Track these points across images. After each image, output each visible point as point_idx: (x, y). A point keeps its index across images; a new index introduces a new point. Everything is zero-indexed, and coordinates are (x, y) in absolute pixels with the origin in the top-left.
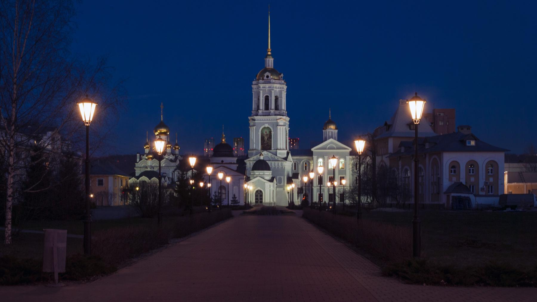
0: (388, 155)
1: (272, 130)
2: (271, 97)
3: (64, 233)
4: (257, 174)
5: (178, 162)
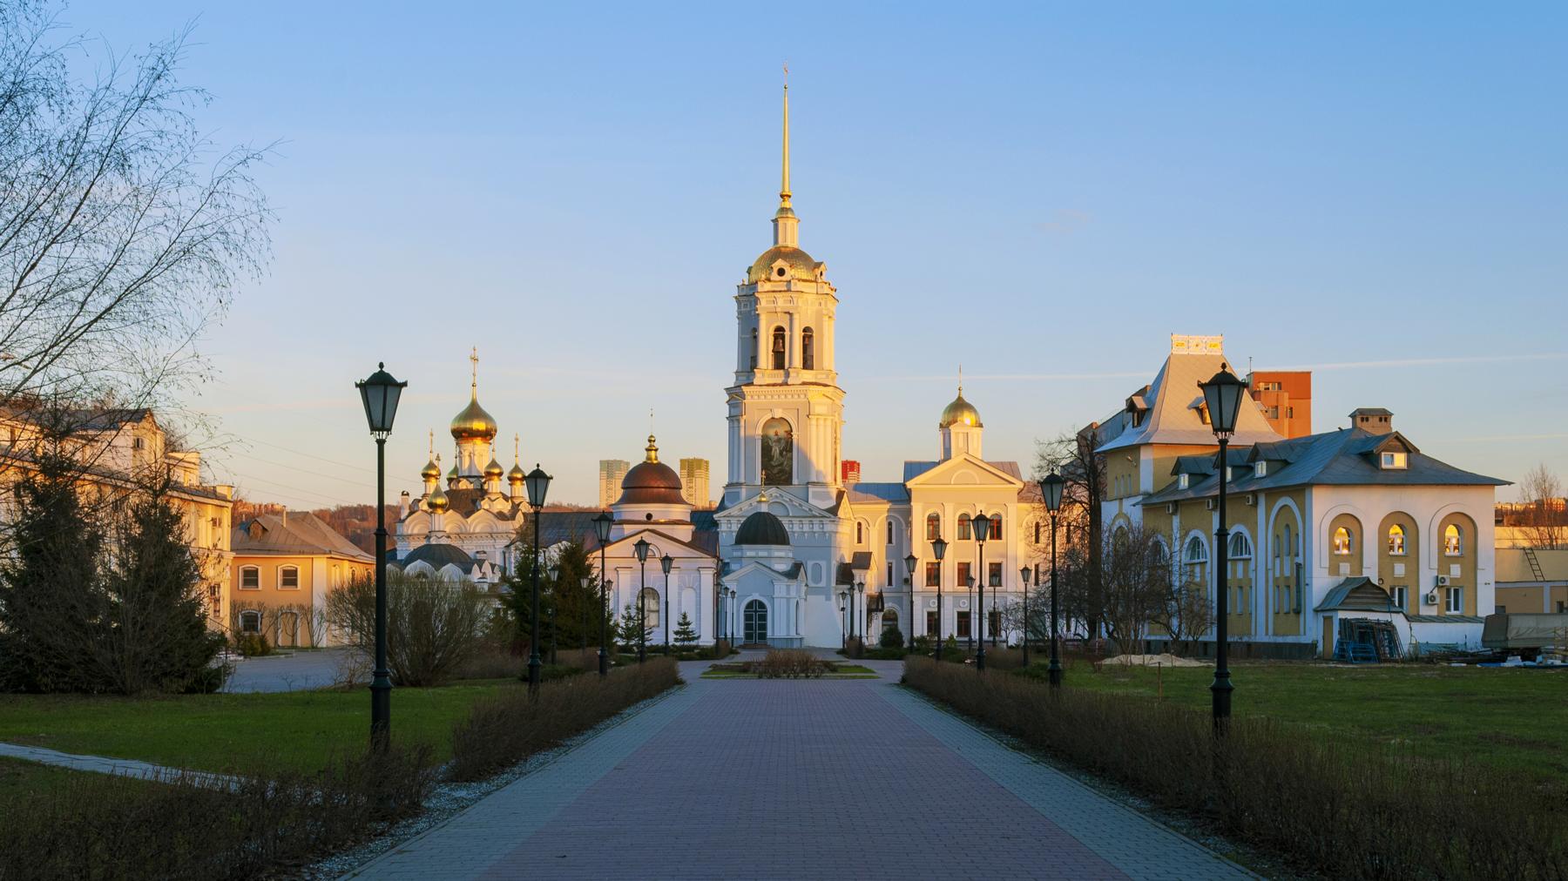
0: (1140, 498)
1: (794, 430)
4: (749, 554)
5: (520, 518)
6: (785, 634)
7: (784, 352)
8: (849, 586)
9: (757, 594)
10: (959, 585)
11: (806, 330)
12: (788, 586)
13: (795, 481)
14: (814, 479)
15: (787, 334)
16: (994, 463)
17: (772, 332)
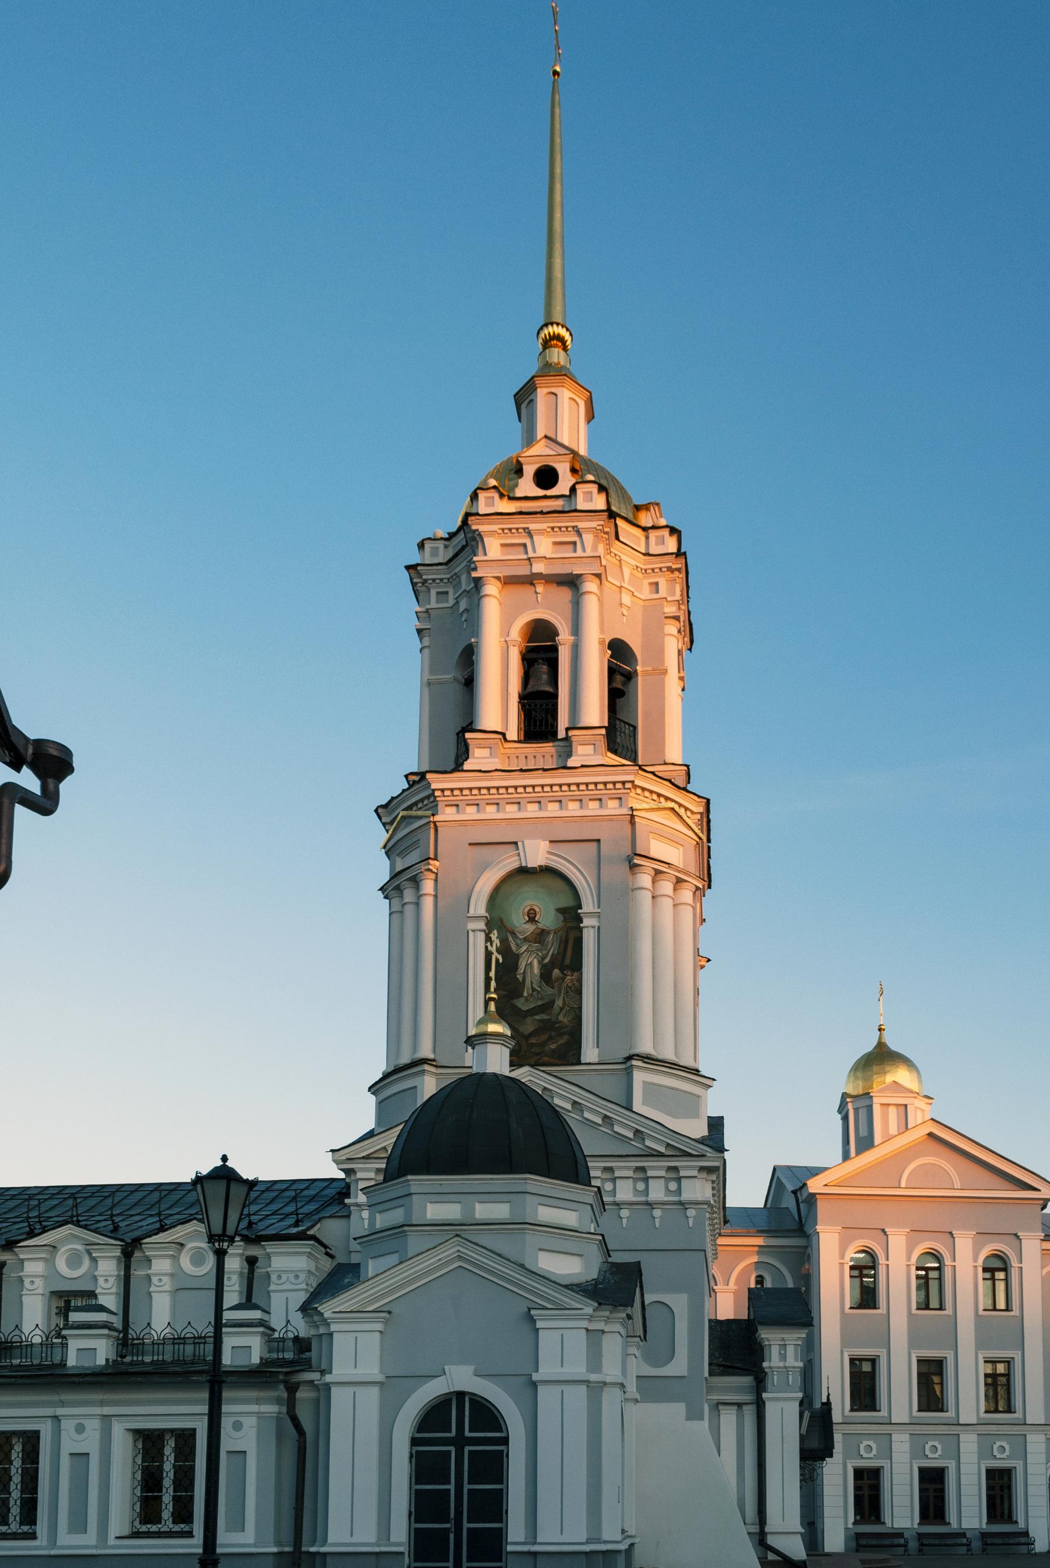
1: (588, 905)
2: (576, 629)
3: (789, 1287)
4: (435, 1211)
6: (372, 1538)
7: (554, 696)
8: (747, 1380)
9: (469, 1370)
10: (920, 1410)
11: (619, 650)
12: (594, 1337)
13: (590, 1053)
14: (646, 1047)
15: (564, 637)
16: (841, 1247)
17: (516, 633)
